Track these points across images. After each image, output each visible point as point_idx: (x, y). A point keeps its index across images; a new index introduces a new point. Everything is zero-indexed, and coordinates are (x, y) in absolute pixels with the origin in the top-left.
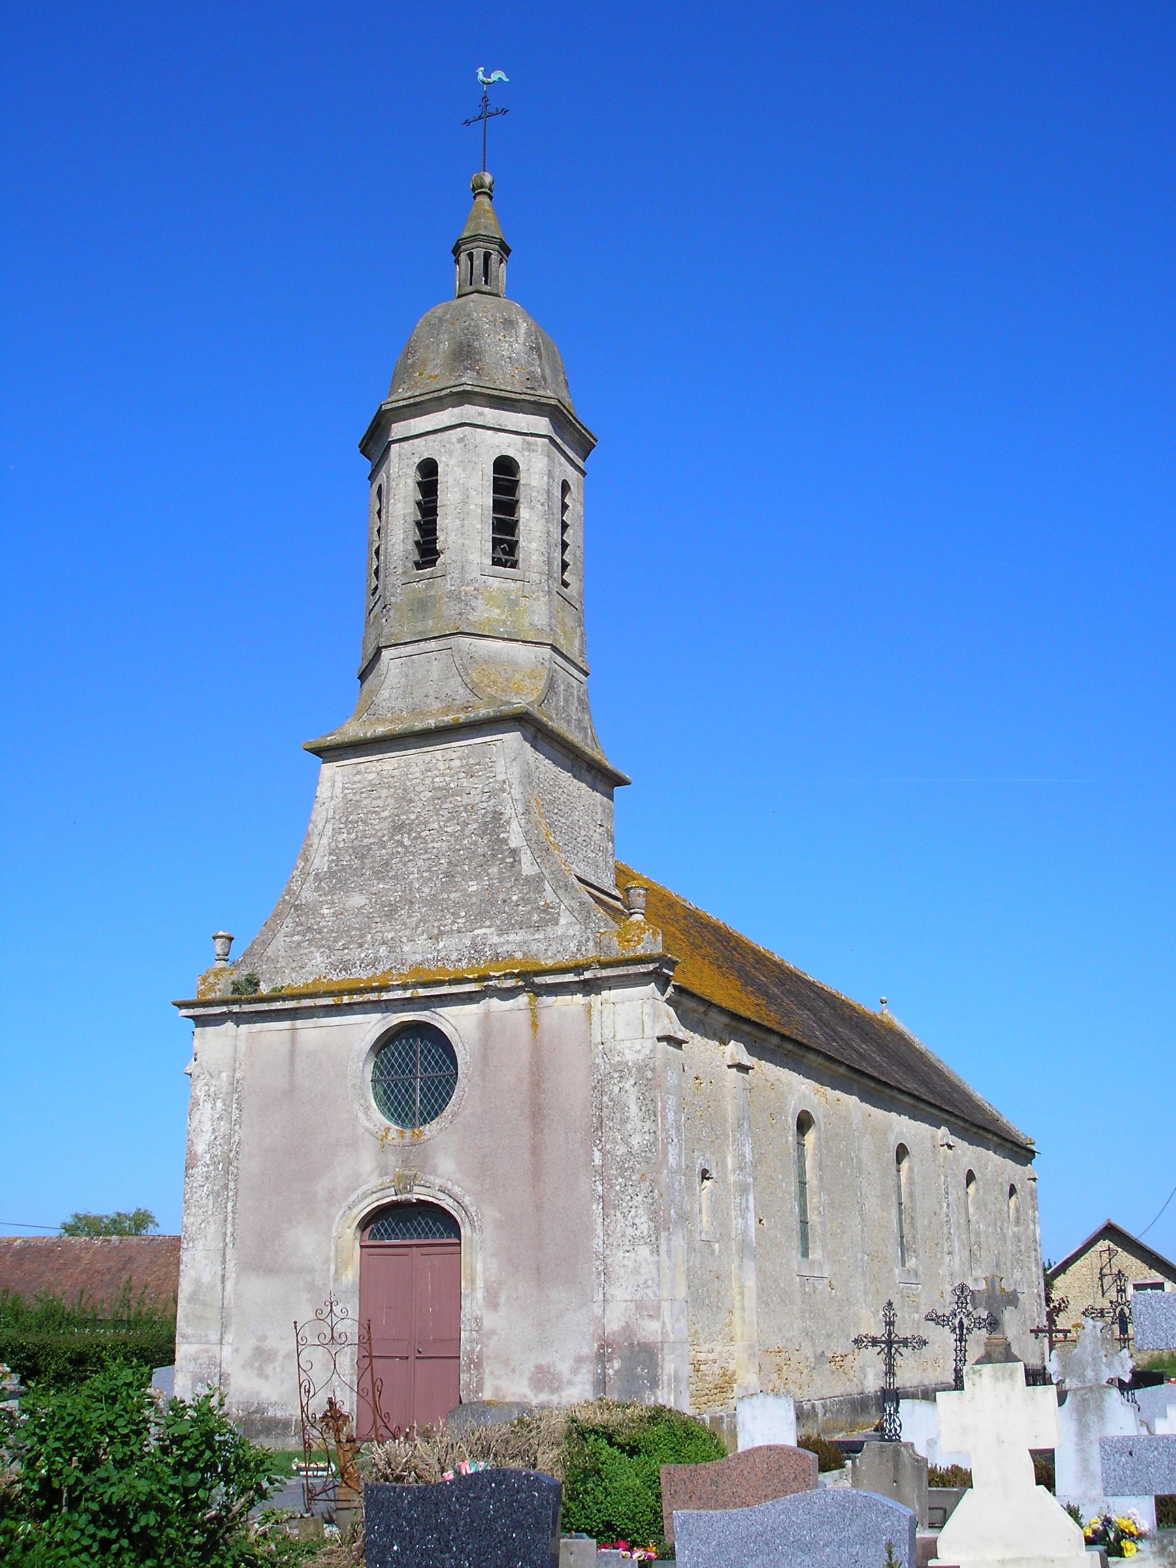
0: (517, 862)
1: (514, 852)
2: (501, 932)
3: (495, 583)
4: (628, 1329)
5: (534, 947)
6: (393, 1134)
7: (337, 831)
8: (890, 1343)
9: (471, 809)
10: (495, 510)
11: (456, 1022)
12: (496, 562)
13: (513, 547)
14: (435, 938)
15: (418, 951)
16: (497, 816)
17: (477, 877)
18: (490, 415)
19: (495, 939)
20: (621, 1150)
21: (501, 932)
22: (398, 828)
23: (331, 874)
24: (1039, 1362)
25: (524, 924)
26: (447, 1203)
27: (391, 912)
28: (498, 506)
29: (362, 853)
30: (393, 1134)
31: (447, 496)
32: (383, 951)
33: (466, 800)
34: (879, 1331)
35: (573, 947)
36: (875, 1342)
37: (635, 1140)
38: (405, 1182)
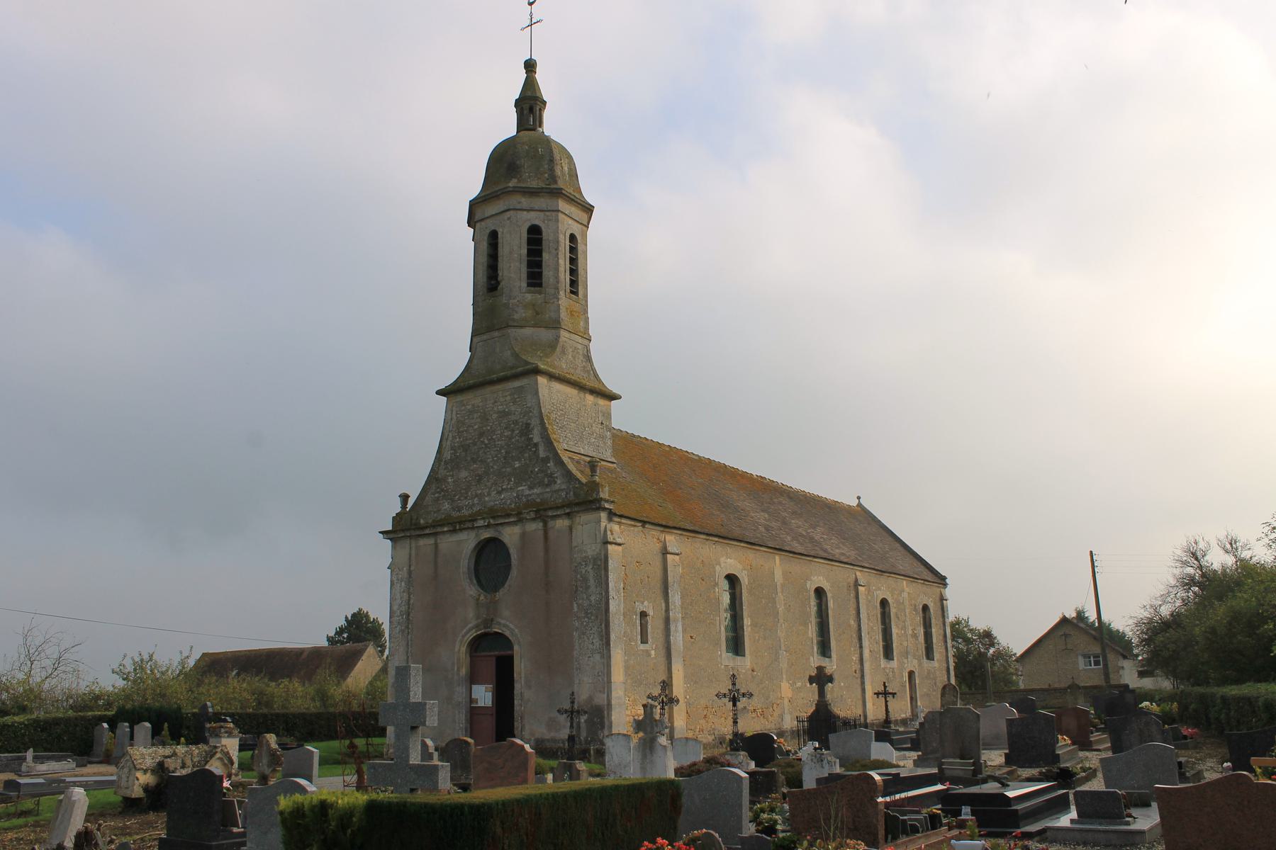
0: (537, 450)
1: (536, 445)
2: (531, 488)
3: (529, 297)
4: (591, 698)
5: (546, 496)
6: (482, 598)
7: (454, 437)
8: (572, 712)
9: (516, 422)
10: (529, 255)
11: (510, 535)
12: (529, 285)
13: (540, 275)
14: (499, 493)
15: (492, 499)
16: (528, 425)
17: (519, 459)
18: (525, 201)
19: (527, 492)
20: (586, 603)
21: (531, 488)
22: (481, 434)
23: (451, 460)
24: (860, 712)
25: (541, 484)
26: (507, 633)
27: (479, 479)
28: (530, 253)
29: (466, 448)
30: (482, 598)
31: (503, 251)
32: (476, 501)
33: (513, 418)
34: (567, 706)
35: (563, 494)
36: (566, 711)
37: (593, 598)
38: (488, 622)
